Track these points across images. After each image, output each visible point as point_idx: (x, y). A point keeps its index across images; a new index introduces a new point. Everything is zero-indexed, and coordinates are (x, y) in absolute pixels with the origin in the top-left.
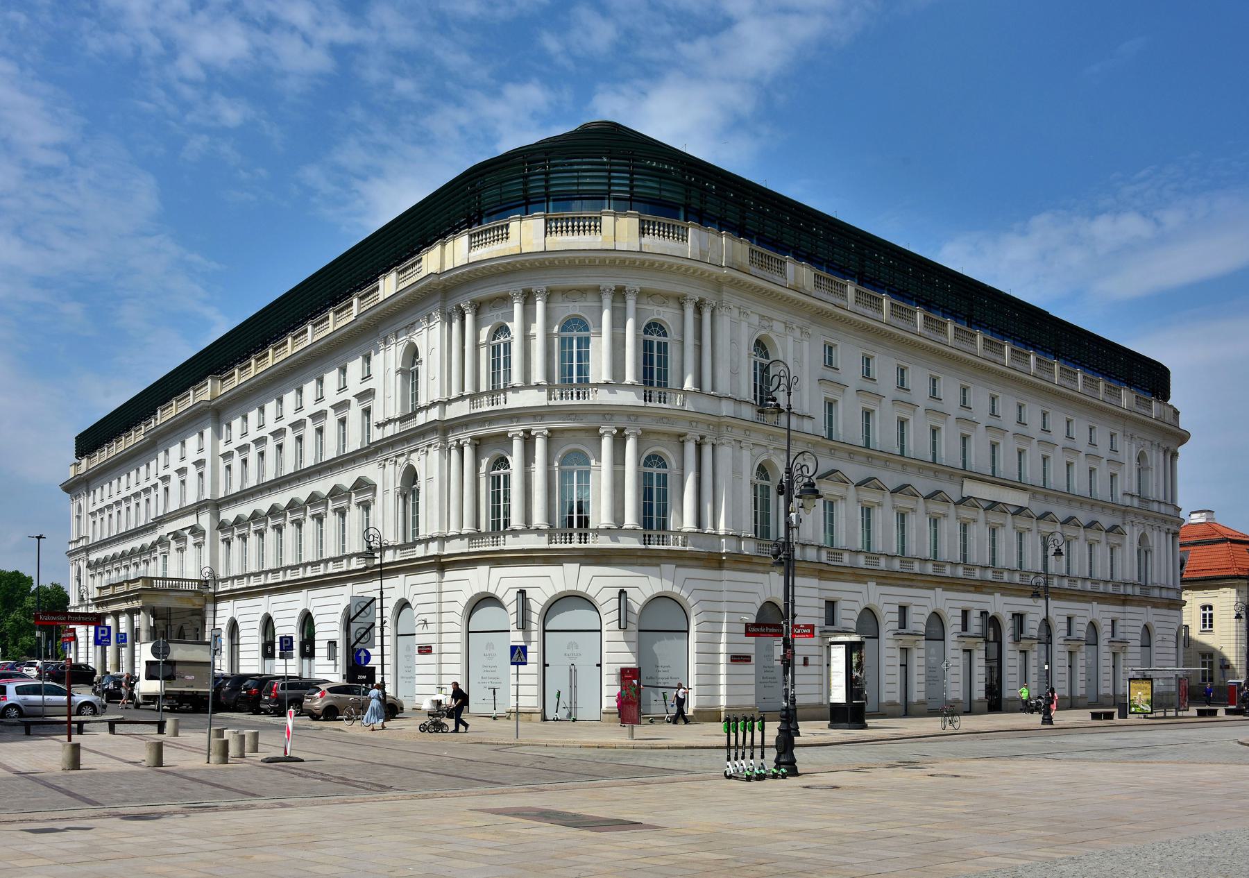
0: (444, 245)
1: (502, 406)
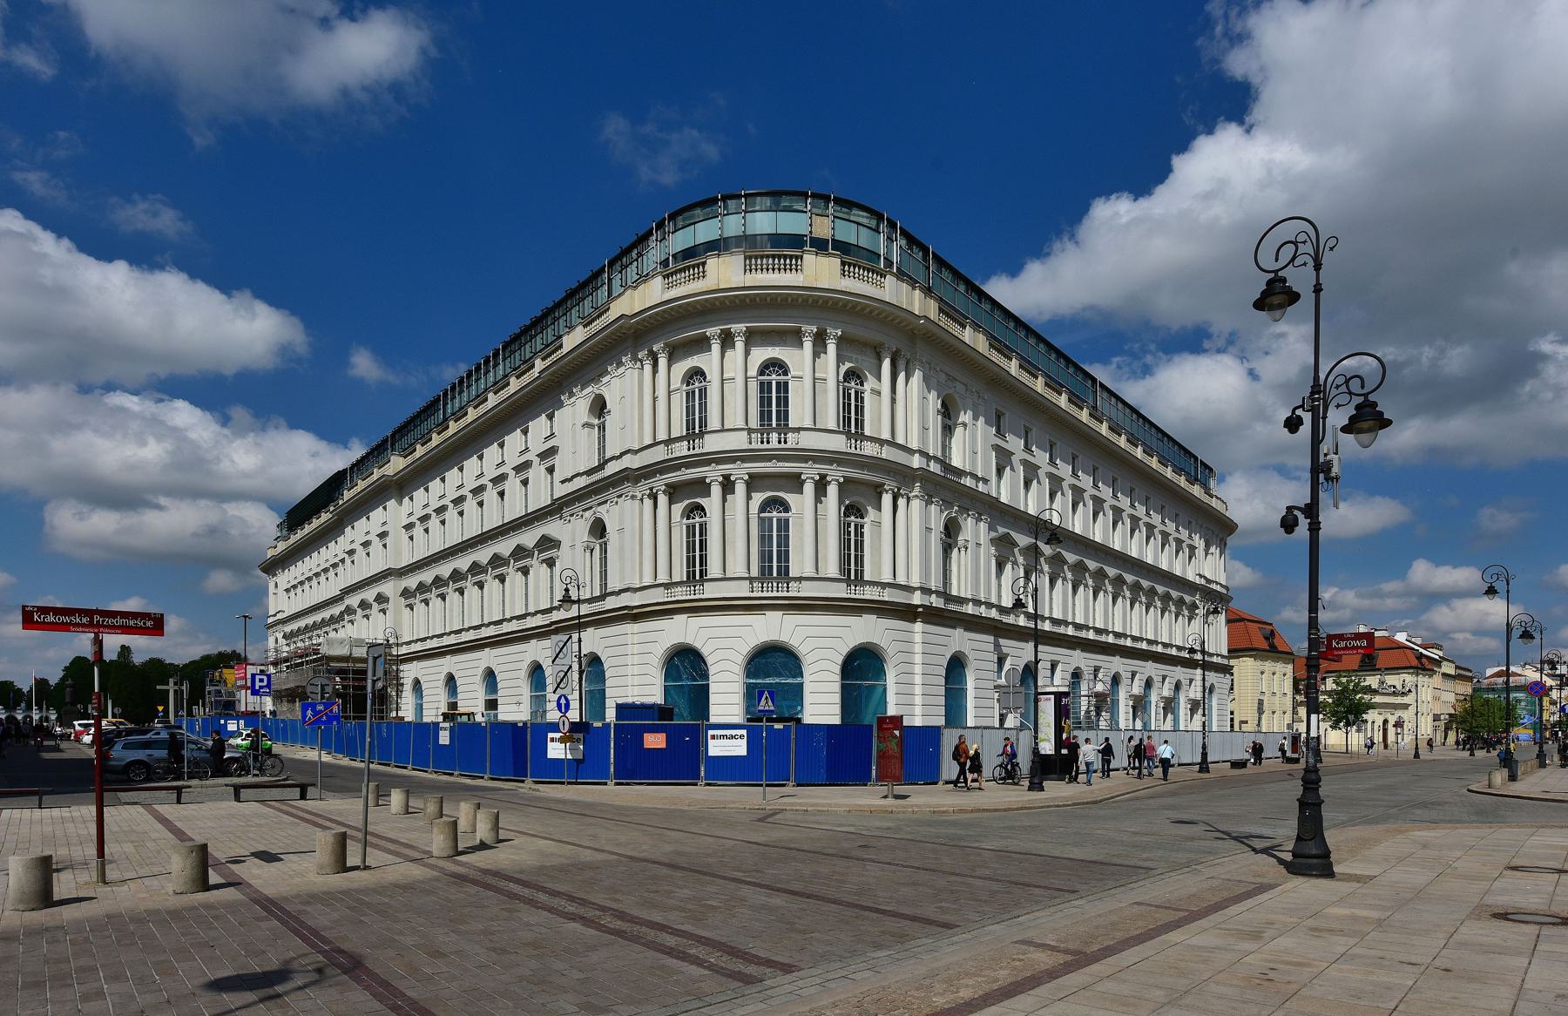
1: (697, 451)
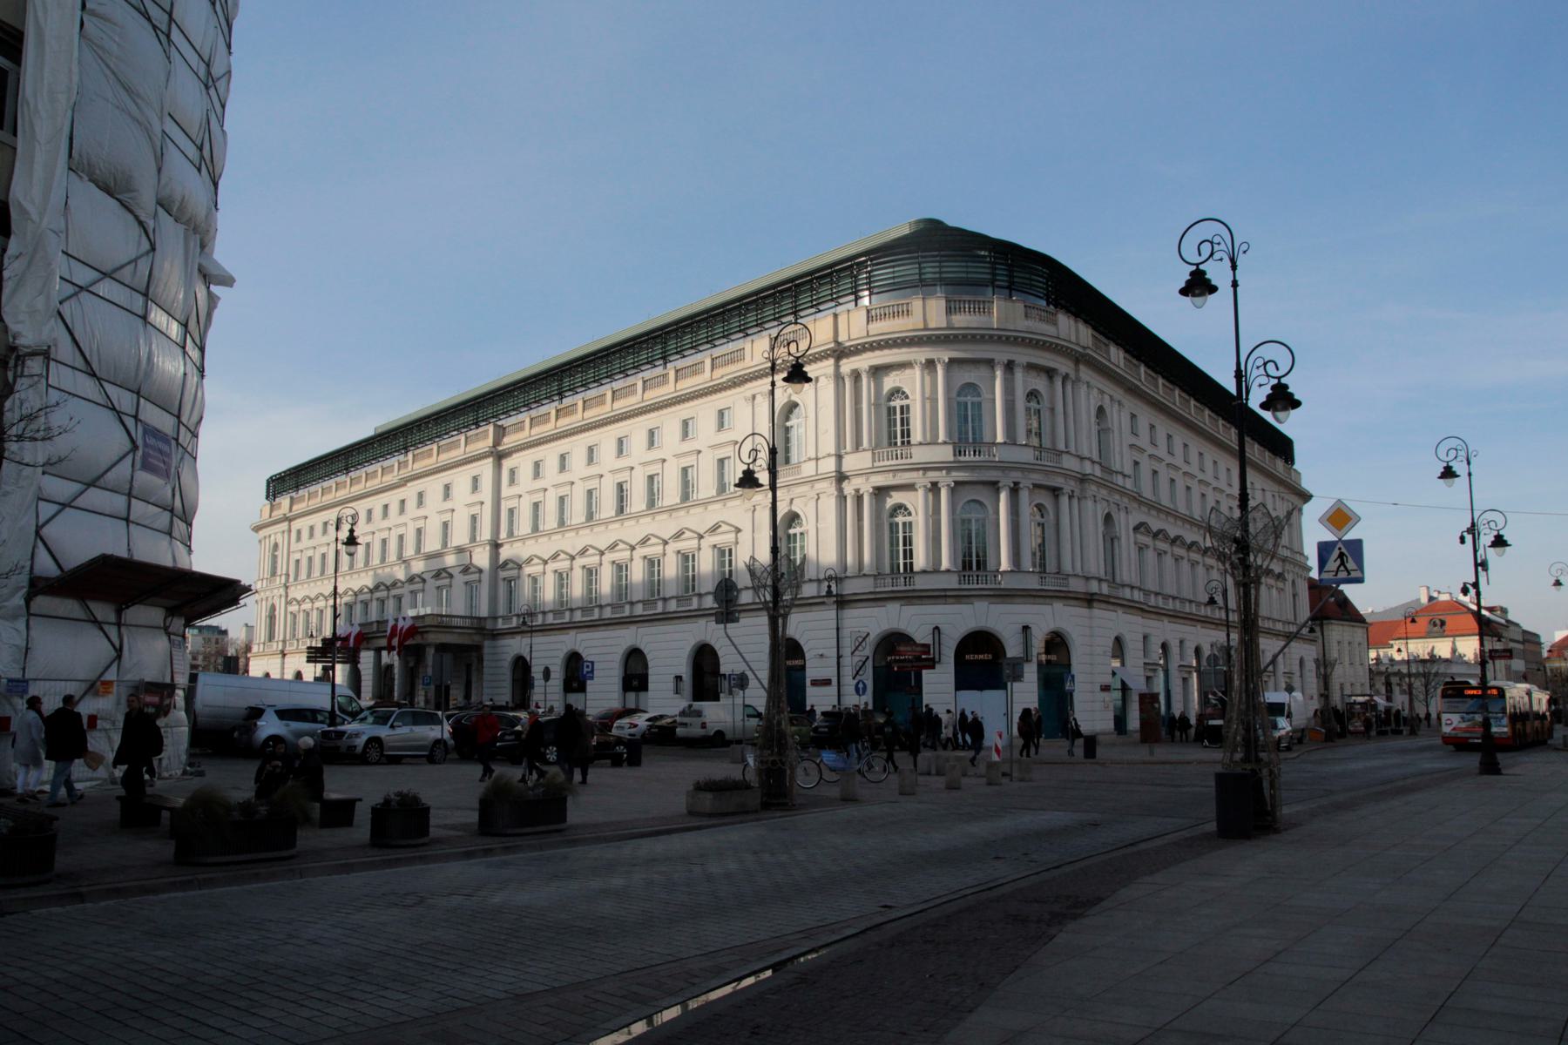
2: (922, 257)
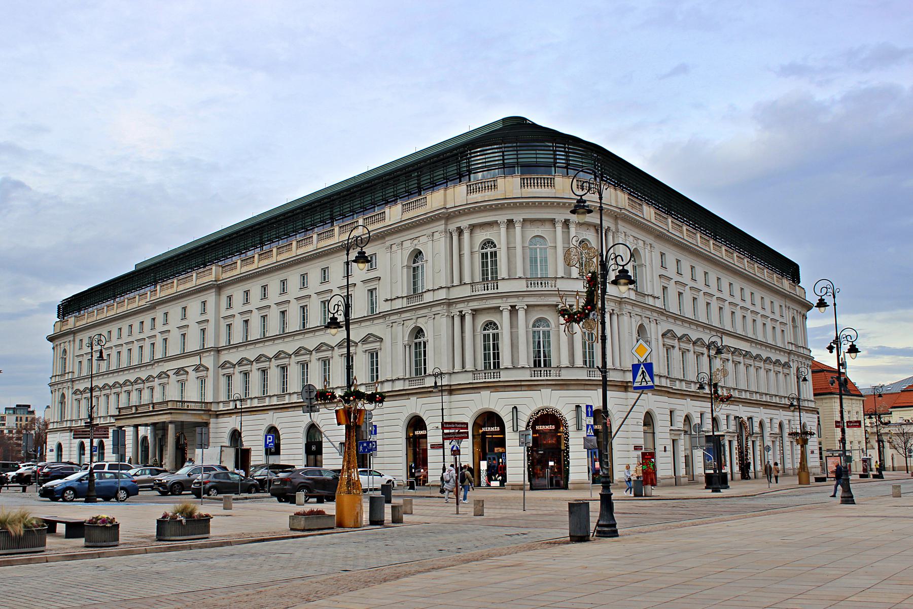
0: (446, 189)
2: (505, 147)
